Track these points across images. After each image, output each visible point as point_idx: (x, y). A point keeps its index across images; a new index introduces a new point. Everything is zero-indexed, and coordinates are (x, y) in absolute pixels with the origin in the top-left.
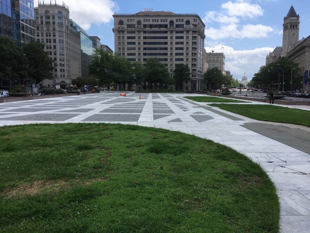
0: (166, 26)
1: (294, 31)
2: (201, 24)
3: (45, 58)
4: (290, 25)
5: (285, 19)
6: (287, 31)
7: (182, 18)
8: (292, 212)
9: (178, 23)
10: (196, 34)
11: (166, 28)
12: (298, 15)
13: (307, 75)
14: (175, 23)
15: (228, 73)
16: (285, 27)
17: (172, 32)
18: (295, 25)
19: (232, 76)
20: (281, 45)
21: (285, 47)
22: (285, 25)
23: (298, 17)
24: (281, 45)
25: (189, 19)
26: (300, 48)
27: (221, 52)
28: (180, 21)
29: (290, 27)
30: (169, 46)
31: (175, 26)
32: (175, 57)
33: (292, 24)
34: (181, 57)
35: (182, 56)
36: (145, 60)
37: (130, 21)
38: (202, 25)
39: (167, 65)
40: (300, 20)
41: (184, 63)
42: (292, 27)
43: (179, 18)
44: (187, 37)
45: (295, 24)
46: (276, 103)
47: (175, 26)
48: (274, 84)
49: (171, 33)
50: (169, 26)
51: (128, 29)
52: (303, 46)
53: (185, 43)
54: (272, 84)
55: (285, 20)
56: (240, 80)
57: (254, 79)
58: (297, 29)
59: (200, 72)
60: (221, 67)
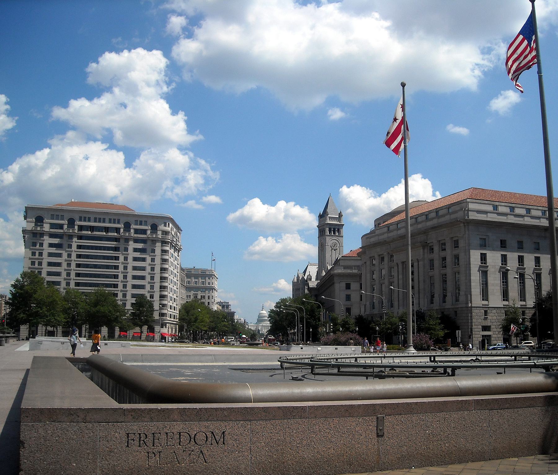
0: (117, 230)
8: (19, 212)
10: (167, 246)
15: (225, 305)
16: (320, 230)
21: (322, 265)
25: (156, 221)
33: (331, 227)
34: (138, 255)
37: (60, 217)
39: (116, 295)
41: (145, 292)
43: (98, 217)
45: (337, 227)
46: (540, 360)
48: (332, 327)
49: (125, 242)
50: (122, 230)
54: (332, 330)
59: (173, 308)
60: (211, 297)
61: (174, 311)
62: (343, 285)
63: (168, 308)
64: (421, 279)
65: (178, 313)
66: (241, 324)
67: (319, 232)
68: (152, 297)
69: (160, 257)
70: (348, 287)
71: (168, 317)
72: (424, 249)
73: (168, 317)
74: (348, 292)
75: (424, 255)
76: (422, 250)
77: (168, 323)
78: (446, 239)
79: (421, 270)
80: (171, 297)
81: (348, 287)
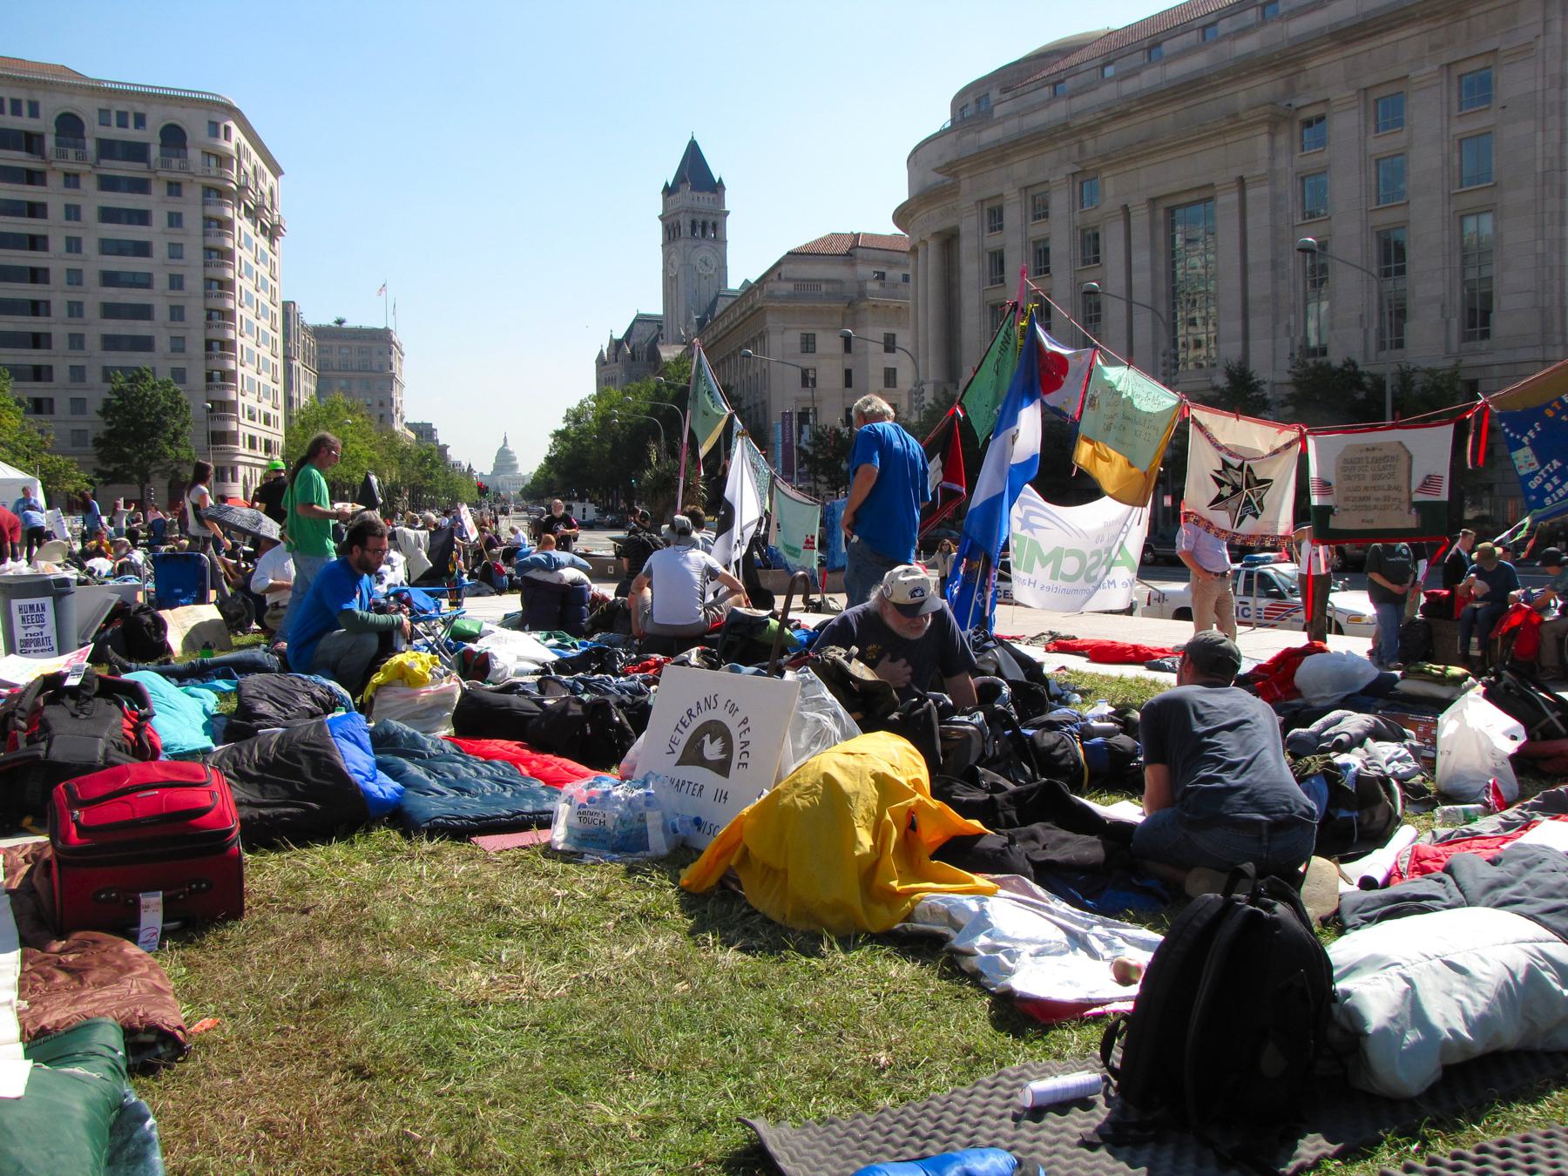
1: (704, 251)
2: (255, 156)
3: (552, 480)
4: (688, 222)
5: (668, 191)
6: (680, 244)
7: (140, 108)
9: (114, 132)
11: (29, 149)
12: (720, 179)
13: (792, 439)
14: (94, 131)
15: (425, 431)
17: (72, 180)
18: (710, 224)
19: (445, 447)
20: (655, 307)
22: (1021, 168)
23: (717, 188)
24: (655, 307)
25: (178, 116)
26: (743, 314)
27: (381, 326)
28: (122, 124)
29: (689, 229)
30: (55, 260)
31: (91, 146)
32: (96, 328)
34: (140, 328)
35: (147, 323)
36: (107, 374)
38: (261, 163)
40: (731, 201)
41: (159, 364)
42: (699, 231)
44: (175, 220)
47: (91, 146)
51: (104, 162)
52: (752, 306)
53: (160, 250)
55: (669, 195)
56: (484, 466)
57: (183, 646)
58: (721, 241)
61: (266, 428)
62: (794, 338)
63: (240, 415)
64: (1259, 254)
65: (283, 433)
66: (463, 473)
67: (664, 233)
68: (179, 375)
69: (199, 241)
70: (808, 344)
71: (241, 444)
72: (1272, 135)
73: (241, 444)
74: (807, 361)
75: (1272, 159)
76: (1263, 141)
77: (245, 464)
78: (1412, 75)
79: (1259, 221)
80: (251, 380)
81: (808, 344)
